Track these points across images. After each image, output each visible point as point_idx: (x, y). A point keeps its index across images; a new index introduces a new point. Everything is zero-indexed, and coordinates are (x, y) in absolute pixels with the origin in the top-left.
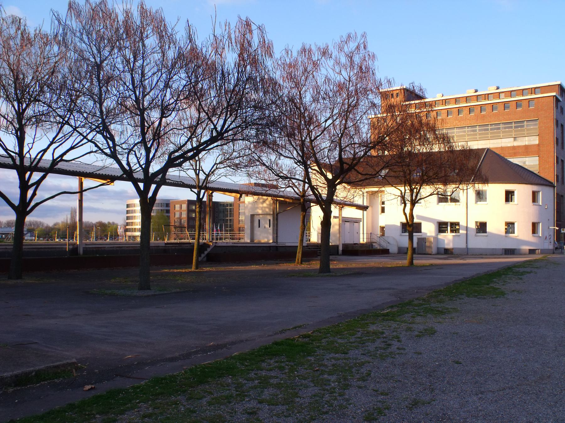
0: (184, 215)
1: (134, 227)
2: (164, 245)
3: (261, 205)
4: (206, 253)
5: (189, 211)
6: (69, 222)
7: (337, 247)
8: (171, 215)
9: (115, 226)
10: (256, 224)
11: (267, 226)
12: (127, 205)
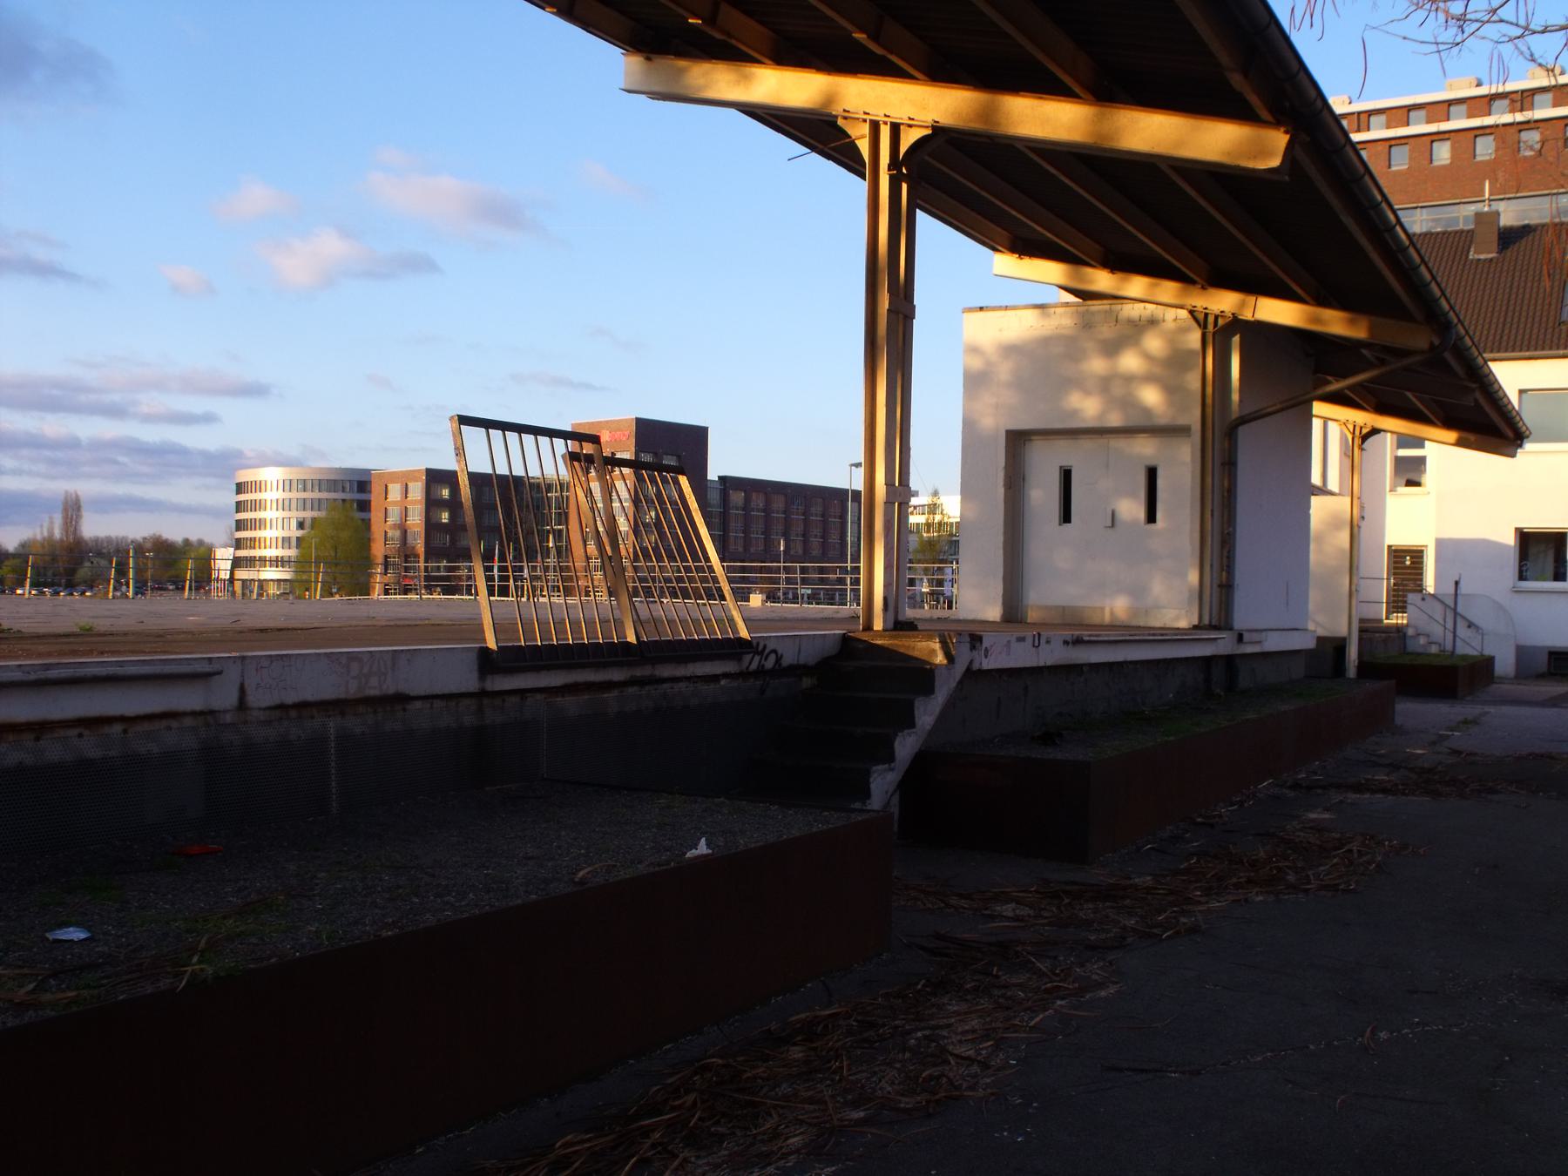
0: (416, 520)
1: (257, 553)
2: (464, 679)
3: (1097, 365)
4: (906, 746)
5: (432, 503)
6: (58, 534)
7: (1339, 646)
8: (376, 516)
9: (202, 550)
10: (1042, 495)
11: (1131, 509)
12: (239, 485)
